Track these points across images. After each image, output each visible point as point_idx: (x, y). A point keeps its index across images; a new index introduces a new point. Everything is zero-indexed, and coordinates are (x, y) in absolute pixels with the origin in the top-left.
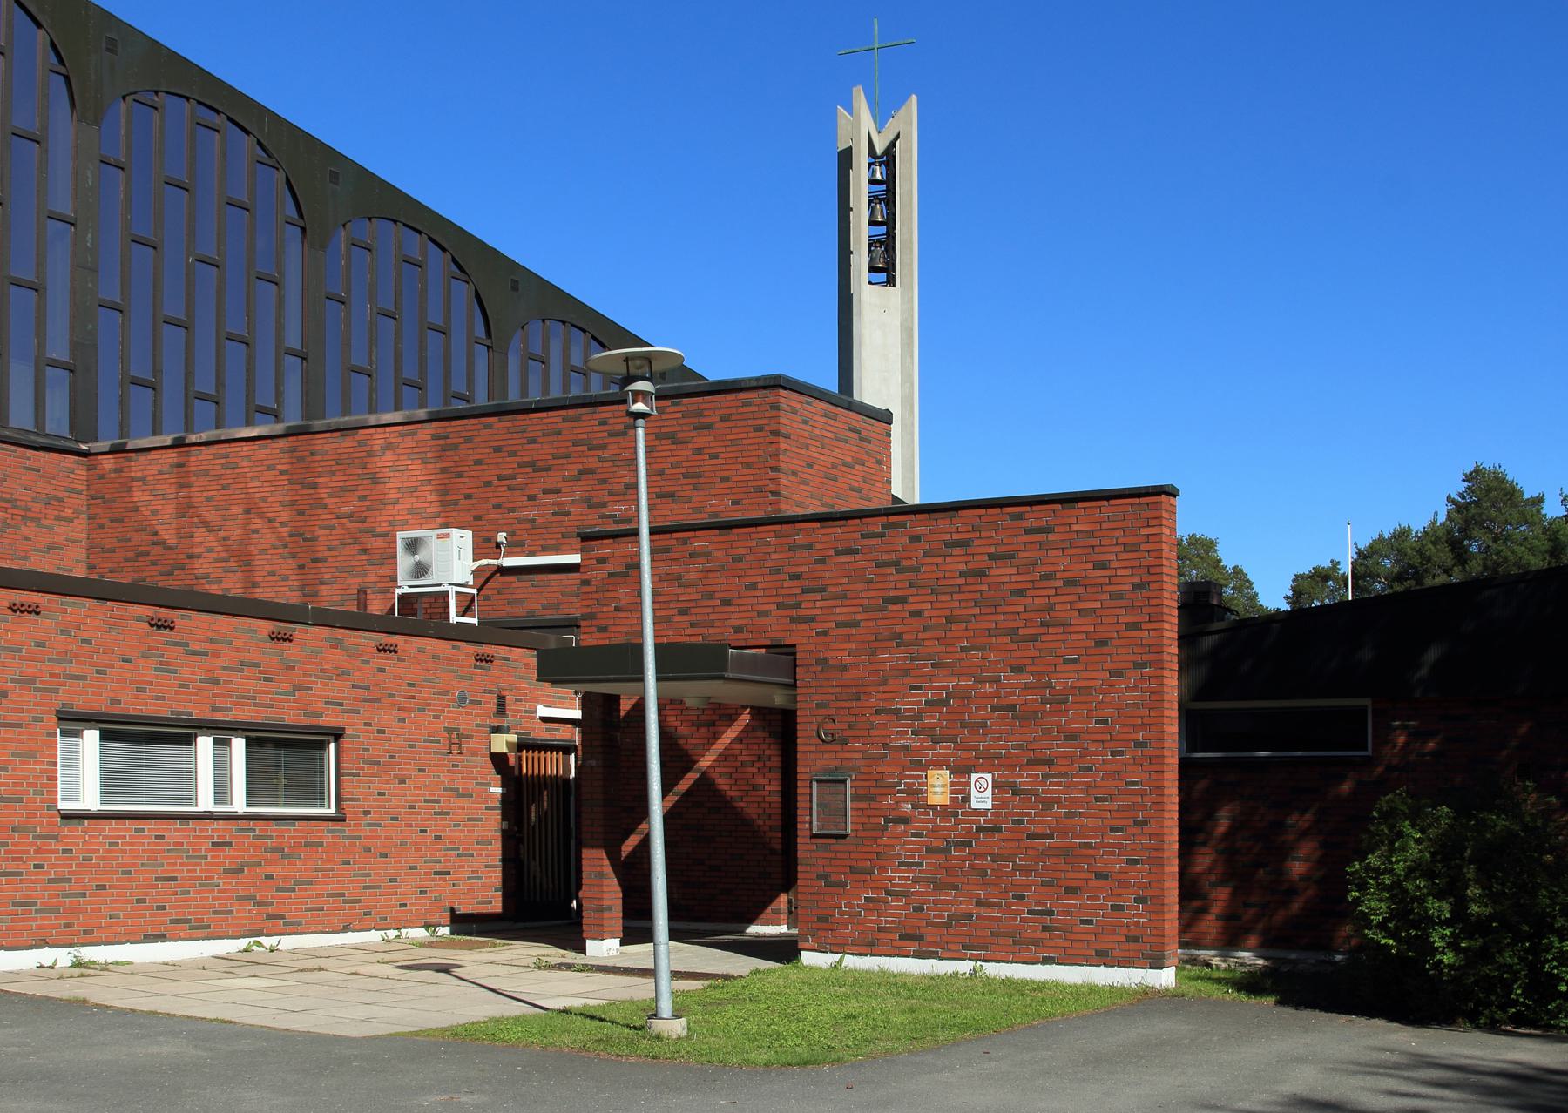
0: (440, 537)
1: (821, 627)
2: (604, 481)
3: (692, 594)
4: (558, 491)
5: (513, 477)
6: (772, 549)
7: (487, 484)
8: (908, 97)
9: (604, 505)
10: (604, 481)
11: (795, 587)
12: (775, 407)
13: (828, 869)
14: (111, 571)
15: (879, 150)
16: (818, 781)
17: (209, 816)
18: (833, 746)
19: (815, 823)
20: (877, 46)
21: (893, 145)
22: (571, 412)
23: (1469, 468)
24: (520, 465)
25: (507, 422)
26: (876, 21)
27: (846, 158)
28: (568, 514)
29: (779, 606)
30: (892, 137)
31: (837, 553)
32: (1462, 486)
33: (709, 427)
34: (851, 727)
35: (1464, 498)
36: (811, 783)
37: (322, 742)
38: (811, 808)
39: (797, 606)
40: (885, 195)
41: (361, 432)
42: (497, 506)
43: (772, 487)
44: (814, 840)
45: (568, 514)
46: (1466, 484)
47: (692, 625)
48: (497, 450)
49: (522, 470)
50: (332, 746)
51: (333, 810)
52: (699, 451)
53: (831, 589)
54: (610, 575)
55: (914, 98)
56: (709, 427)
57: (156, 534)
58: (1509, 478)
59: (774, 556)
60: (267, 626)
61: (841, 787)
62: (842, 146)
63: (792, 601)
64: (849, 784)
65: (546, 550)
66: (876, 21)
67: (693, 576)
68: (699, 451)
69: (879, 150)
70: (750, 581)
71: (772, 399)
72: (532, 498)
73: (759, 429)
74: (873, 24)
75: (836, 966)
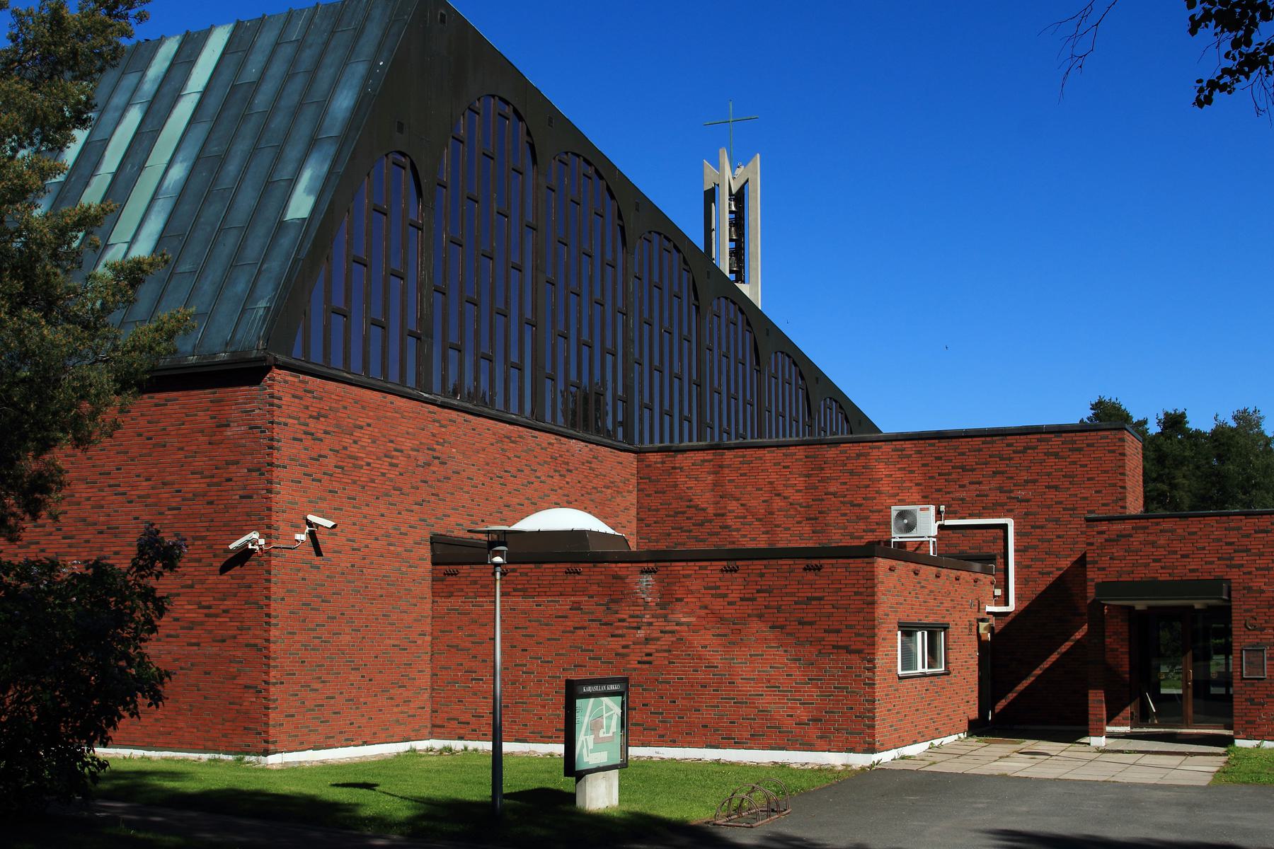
0: (921, 509)
1: (1246, 570)
2: (1012, 478)
3: (1162, 552)
4: (980, 483)
5: (949, 474)
6: (1214, 529)
7: (932, 477)
8: (754, 155)
9: (1011, 491)
10: (1012, 478)
11: (1230, 549)
12: (1122, 440)
13: (1253, 696)
14: (655, 523)
15: (734, 191)
16: (1246, 650)
17: (924, 675)
18: (1253, 632)
19: (1244, 672)
20: (731, 120)
21: (742, 188)
22: (988, 439)
23: (1095, 400)
24: (953, 468)
25: (944, 443)
26: (731, 104)
27: (710, 196)
28: (987, 496)
29: (1219, 559)
30: (743, 182)
31: (1256, 532)
32: (1090, 413)
33: (1080, 450)
34: (1266, 622)
35: (1092, 421)
36: (1242, 651)
37: (912, 631)
38: (1242, 665)
39: (1231, 559)
40: (738, 222)
41: (842, 445)
42: (937, 490)
43: (1121, 484)
44: (1243, 681)
45: (987, 496)
46: (1093, 411)
47: (1162, 568)
48: (937, 458)
49: (955, 470)
50: (943, 633)
51: (943, 669)
52: (1075, 463)
53: (1253, 551)
54: (1106, 540)
55: (758, 155)
56: (1080, 450)
57: (691, 501)
58: (1123, 408)
59: (1216, 533)
60: (802, 563)
61: (1261, 653)
62: (708, 187)
63: (1228, 556)
64: (1265, 652)
65: (971, 516)
66: (731, 104)
67: (1162, 542)
68: (1075, 463)
69: (734, 191)
70: (1200, 545)
71: (1121, 436)
72: (964, 486)
73: (1114, 451)
74: (729, 106)
75: (1258, 746)
